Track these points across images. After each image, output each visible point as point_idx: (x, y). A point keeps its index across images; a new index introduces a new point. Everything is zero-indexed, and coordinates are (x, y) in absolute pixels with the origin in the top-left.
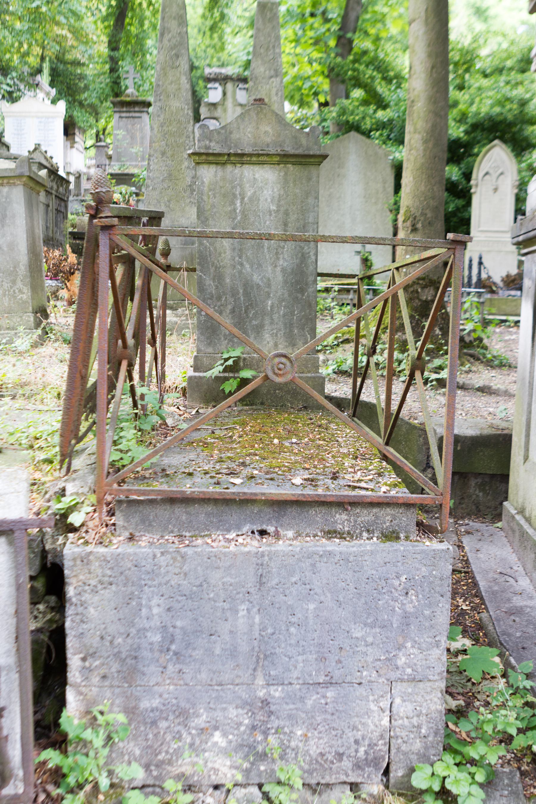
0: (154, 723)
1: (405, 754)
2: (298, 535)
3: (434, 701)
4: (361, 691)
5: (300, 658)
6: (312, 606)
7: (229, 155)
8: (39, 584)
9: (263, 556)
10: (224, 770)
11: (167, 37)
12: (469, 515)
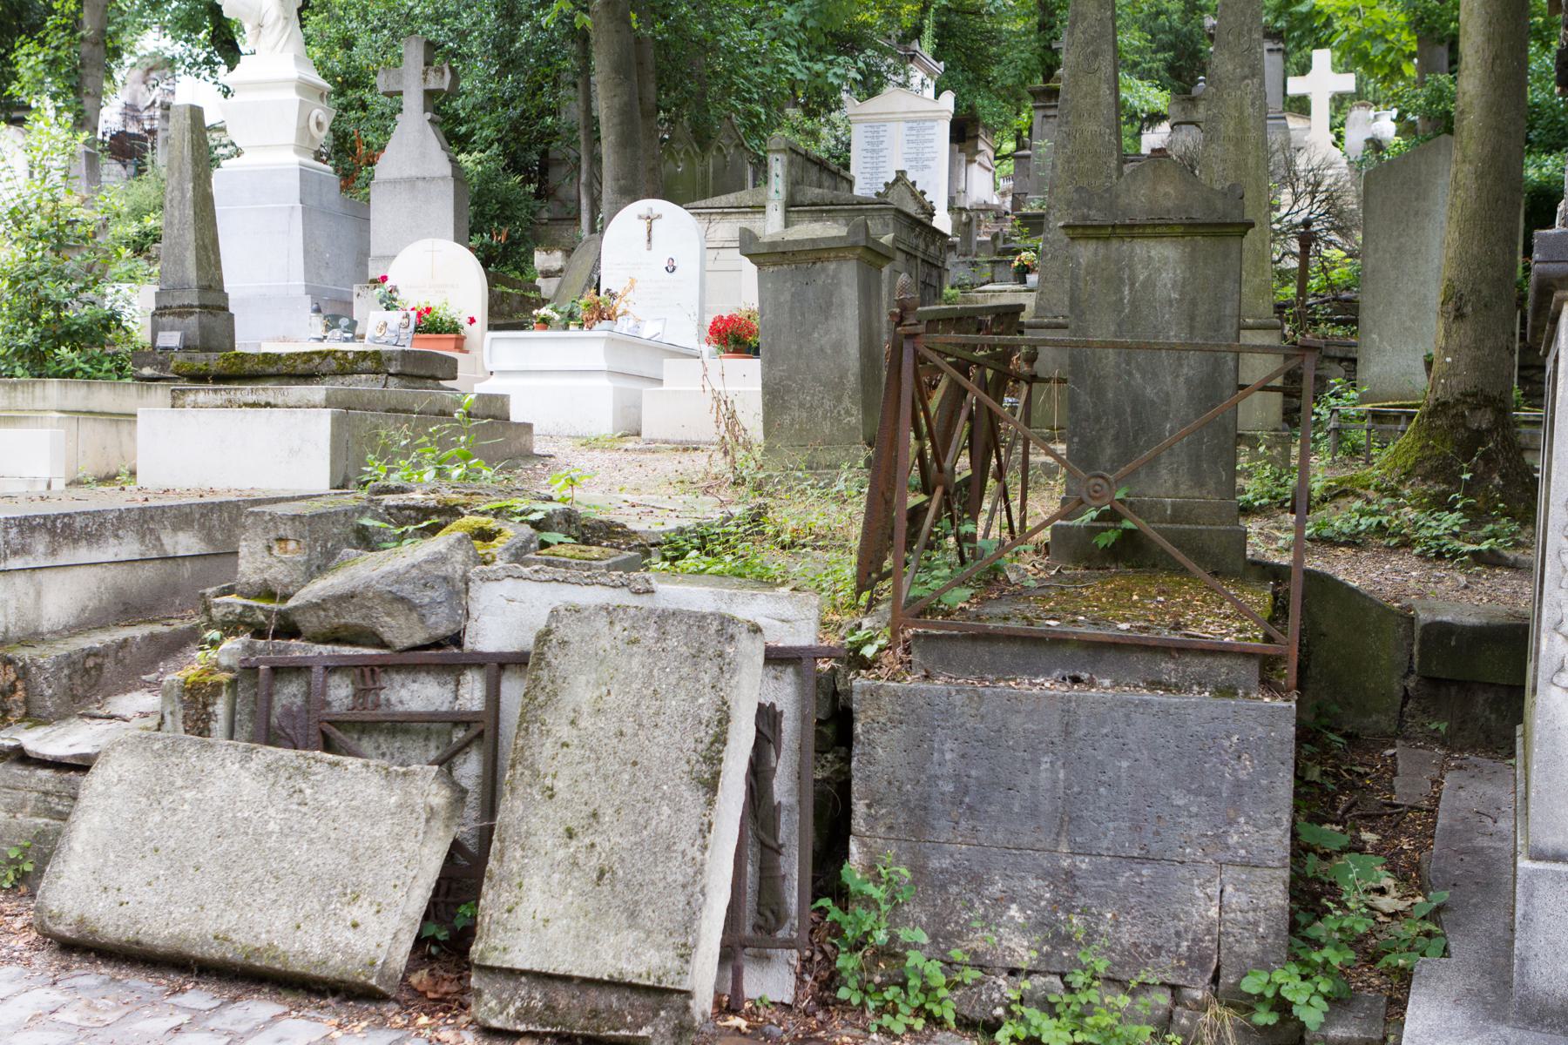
0: (943, 887)
1: (1238, 956)
2: (1116, 683)
3: (1276, 896)
4: (1184, 872)
5: (1111, 825)
6: (1125, 764)
7: (1113, 226)
8: (828, 731)
9: (1070, 701)
10: (1022, 951)
11: (1080, 27)
12: (1473, 748)
